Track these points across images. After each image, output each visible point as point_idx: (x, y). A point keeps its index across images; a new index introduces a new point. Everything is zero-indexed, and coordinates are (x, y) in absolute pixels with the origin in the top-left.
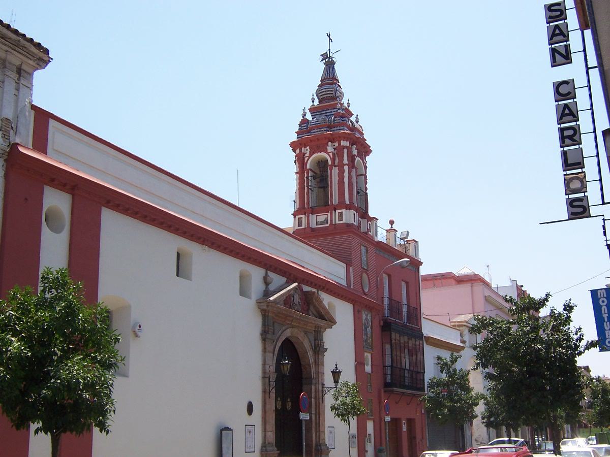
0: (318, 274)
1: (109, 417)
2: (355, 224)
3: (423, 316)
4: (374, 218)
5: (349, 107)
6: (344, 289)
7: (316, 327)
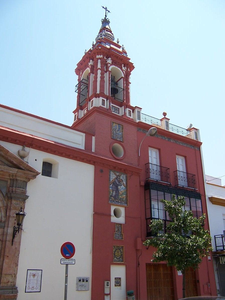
0: (38, 137)
1: (164, 261)
2: (105, 107)
3: (206, 182)
4: (136, 107)
5: (118, 43)
6: (76, 151)
7: (10, 175)
